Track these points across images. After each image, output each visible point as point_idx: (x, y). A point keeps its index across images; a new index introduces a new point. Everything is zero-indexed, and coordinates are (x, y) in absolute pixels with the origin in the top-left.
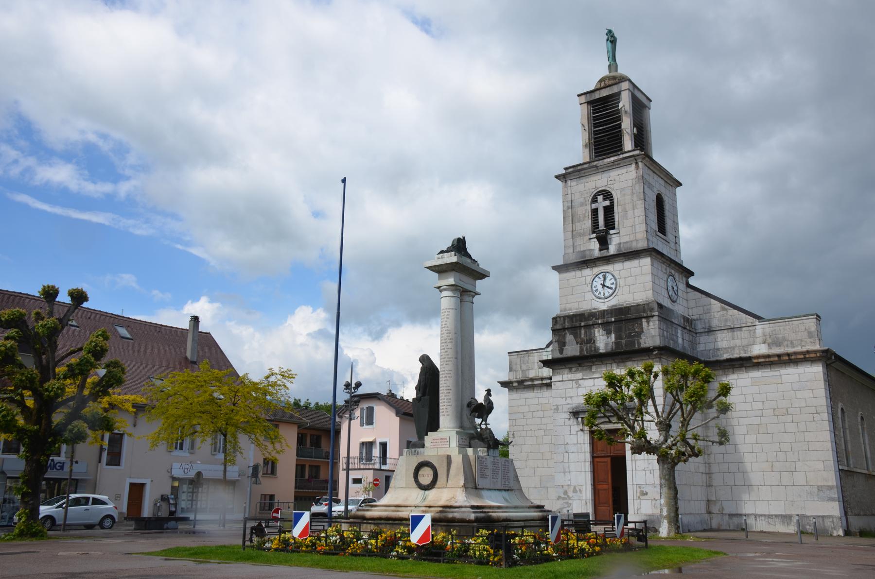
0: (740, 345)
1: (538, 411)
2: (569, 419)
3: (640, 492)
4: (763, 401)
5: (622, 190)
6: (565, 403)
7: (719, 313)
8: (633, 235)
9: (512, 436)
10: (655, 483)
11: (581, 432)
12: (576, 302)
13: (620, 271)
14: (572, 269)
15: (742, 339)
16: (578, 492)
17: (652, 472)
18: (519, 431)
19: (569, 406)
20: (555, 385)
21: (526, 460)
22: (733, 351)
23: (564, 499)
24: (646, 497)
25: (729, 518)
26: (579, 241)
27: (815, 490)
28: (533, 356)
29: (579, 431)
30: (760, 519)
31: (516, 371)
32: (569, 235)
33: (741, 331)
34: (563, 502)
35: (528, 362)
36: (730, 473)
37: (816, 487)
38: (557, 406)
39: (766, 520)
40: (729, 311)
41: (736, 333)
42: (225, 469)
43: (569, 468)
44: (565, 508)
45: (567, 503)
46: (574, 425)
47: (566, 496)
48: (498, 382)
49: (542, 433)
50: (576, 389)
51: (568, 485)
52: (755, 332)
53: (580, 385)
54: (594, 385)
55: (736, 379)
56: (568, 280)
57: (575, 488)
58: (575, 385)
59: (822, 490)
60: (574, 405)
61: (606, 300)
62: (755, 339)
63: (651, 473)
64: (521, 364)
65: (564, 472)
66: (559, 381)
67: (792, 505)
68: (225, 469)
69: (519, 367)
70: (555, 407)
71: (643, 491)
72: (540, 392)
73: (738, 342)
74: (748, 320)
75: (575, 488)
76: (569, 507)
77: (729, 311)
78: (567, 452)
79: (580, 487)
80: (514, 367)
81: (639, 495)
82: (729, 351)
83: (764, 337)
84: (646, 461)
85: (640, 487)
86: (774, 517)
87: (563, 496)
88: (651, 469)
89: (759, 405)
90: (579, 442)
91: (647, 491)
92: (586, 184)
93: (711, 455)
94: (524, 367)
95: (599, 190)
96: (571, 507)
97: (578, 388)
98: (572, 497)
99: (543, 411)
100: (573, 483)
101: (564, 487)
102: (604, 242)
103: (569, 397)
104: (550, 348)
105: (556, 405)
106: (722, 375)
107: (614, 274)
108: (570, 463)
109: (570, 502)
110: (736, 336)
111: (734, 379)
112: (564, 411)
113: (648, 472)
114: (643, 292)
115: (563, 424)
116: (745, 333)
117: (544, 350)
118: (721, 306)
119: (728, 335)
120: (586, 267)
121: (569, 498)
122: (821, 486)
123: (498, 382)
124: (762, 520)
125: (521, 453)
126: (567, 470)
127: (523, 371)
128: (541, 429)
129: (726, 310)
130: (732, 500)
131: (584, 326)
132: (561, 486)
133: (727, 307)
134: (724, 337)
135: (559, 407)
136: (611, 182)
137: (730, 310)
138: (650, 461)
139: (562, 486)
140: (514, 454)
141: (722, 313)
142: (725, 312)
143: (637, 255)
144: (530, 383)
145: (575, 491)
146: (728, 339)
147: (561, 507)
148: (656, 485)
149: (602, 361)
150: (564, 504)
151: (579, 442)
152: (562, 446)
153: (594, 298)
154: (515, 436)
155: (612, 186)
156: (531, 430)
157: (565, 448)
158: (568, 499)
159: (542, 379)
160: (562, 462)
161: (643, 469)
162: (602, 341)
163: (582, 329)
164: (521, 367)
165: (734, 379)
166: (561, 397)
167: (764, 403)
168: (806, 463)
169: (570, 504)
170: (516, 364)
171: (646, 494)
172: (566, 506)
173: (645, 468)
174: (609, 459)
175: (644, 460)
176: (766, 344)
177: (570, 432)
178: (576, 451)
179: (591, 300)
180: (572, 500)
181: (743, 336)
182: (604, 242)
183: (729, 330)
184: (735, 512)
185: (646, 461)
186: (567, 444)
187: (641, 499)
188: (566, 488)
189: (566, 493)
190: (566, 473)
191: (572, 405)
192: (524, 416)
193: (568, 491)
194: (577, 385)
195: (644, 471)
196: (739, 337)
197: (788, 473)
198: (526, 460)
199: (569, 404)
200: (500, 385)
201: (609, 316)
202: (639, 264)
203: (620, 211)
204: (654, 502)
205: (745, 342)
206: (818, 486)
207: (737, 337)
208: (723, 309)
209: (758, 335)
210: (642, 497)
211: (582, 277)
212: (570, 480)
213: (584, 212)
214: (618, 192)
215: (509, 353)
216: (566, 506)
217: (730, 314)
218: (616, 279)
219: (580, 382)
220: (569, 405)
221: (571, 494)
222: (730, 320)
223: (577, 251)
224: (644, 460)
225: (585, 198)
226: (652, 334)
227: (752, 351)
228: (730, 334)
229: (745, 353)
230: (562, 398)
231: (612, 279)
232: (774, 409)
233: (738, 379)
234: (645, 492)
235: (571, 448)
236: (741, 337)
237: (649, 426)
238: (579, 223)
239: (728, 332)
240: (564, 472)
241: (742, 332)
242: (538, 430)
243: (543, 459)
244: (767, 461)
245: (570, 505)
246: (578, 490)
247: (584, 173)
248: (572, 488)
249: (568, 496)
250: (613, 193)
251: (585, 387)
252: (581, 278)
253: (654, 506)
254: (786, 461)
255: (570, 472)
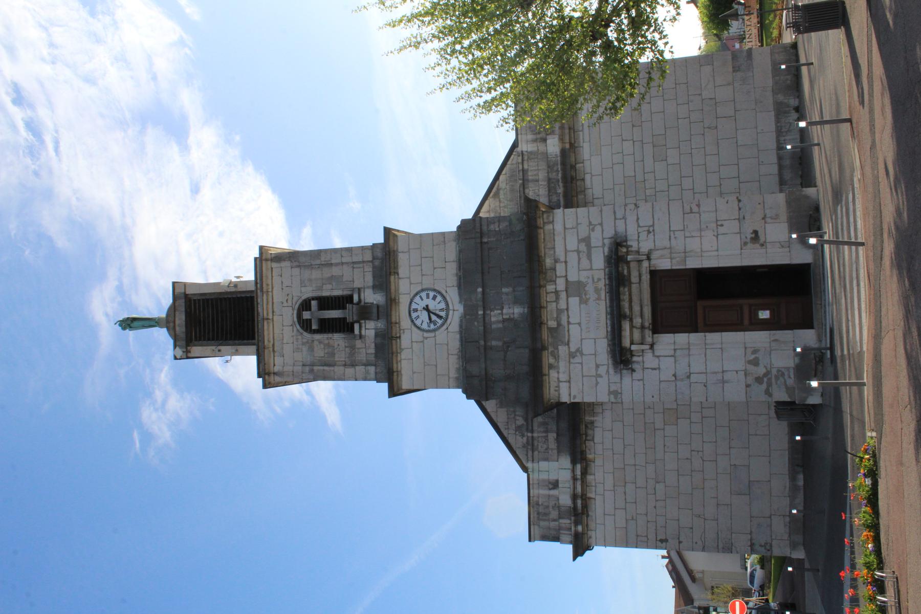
0: (546, 171)
1: (625, 493)
2: (633, 370)
3: (754, 243)
4: (623, 140)
5: (302, 284)
6: (606, 377)
7: (502, 199)
8: (365, 267)
9: (664, 544)
10: (738, 217)
11: (655, 347)
12: (448, 358)
13: (411, 284)
14: (397, 363)
15: (538, 170)
16: (757, 355)
17: (719, 223)
18: (656, 530)
19: (611, 371)
20: (575, 397)
21: (705, 519)
23: (769, 384)
25: (786, 185)
26: (362, 356)
27: (739, 74)
28: (538, 497)
29: (653, 352)
30: (783, 142)
31: (559, 529)
32: (350, 371)
33: (527, 170)
34: (774, 386)
35: (547, 507)
36: (721, 184)
37: (734, 74)
38: (610, 393)
39: (784, 134)
41: (530, 178)
44: (785, 382)
45: (777, 378)
46: (643, 362)
47: (765, 379)
48: (574, 559)
49: (660, 487)
51: (746, 375)
52: (531, 153)
53: (578, 350)
54: (579, 324)
55: (592, 176)
56: (414, 373)
57: (750, 362)
58: (578, 359)
59: (739, 67)
60: (610, 362)
61: (451, 307)
62: (540, 152)
63: (722, 225)
64: (548, 520)
65: (723, 382)
66: (570, 387)
67: (761, 102)
69: (553, 523)
71: (752, 239)
72: (596, 486)
73: (542, 175)
74: (514, 162)
75: (750, 362)
76: (783, 375)
78: (689, 377)
79: (749, 351)
80: (553, 533)
81: (757, 246)
83: (538, 140)
85: (746, 244)
86: (779, 124)
87: (764, 386)
88: (715, 225)
89: (628, 146)
90: (672, 353)
91: (751, 231)
92: (285, 341)
93: (709, 593)
94: (554, 514)
95: (296, 319)
96: (783, 370)
97: (582, 354)
98: (765, 367)
99: (626, 483)
100: (740, 365)
101: (749, 383)
102: (365, 312)
103: (597, 370)
104: (529, 465)
105: (609, 395)
107: (415, 292)
108: (708, 371)
109: (774, 372)
110: (533, 178)
111: (591, 178)
112: (619, 381)
113: (721, 230)
114: (446, 245)
115: (641, 382)
116: (530, 166)
117: (531, 476)
119: (531, 187)
120: (397, 325)
122: (733, 67)
123: (574, 559)
124: (784, 140)
125: (692, 528)
126: (720, 376)
127: (560, 517)
128: (655, 489)
129: (498, 189)
131: (485, 341)
133: (494, 189)
134: (534, 193)
135: (611, 390)
136: (290, 302)
138: (703, 226)
139: (748, 386)
140: (694, 541)
142: (501, 192)
143: (392, 254)
144: (579, 502)
145: (755, 362)
147: (785, 390)
148: (741, 217)
149: (541, 307)
150: (779, 382)
151: (672, 353)
152: (678, 384)
153: (445, 327)
154: (664, 538)
155: (295, 299)
156: (655, 507)
157: (682, 380)
158: (770, 376)
159: (574, 479)
160: (705, 386)
163: (489, 344)
164: (554, 520)
165: (591, 178)
166: (596, 386)
167: (624, 138)
168: (703, 87)
169: (778, 371)
170: (549, 528)
171: (756, 232)
173: (714, 235)
174: (700, 304)
175: (701, 237)
176: (548, 137)
177: (655, 369)
179: (448, 332)
181: (534, 168)
182: (365, 312)
183: (526, 186)
184: (777, 179)
186: (675, 375)
187: (765, 242)
188: (750, 380)
189: (759, 380)
190: (725, 378)
191: (611, 366)
192: (633, 519)
193: (757, 376)
194: (578, 354)
196: (535, 173)
197: (718, 108)
198: (705, 519)
199: (608, 371)
200: (579, 558)
202: (405, 252)
203: (329, 286)
204: (768, 220)
205: (543, 165)
206: (734, 71)
207: (535, 175)
208: (497, 195)
209: (535, 149)
210: (762, 240)
211: (412, 348)
213: (322, 346)
214: (303, 289)
215: (530, 540)
216: (781, 379)
218: (423, 290)
221: (761, 370)
222: (512, 186)
223: (374, 359)
224: (701, 237)
225: (303, 344)
226: (507, 226)
227: (556, 155)
228: (531, 185)
229: (557, 165)
230: (597, 383)
231: (421, 297)
232: (633, 126)
233: (591, 173)
235: (682, 370)
236: (535, 170)
237: (646, 229)
238: (337, 356)
239: (528, 188)
240: (723, 382)
241: (530, 169)
242: (655, 494)
243: (703, 489)
244: (703, 134)
245: (781, 373)
246: (753, 357)
247: (269, 341)
248: (751, 368)
249: (765, 375)
250: (303, 298)
252: (414, 349)
253: (775, 219)
254: (702, 110)
255: (723, 372)
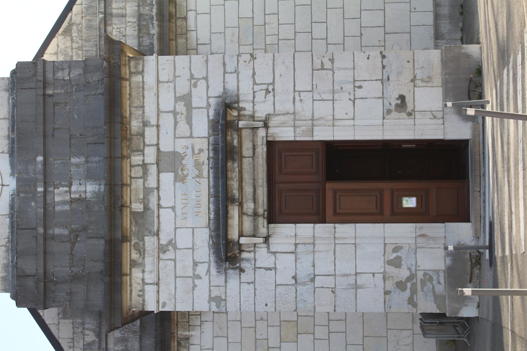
2: (242, 270)
3: (399, 112)
6: (206, 279)
7: (74, 38)
10: (380, 78)
16: (399, 254)
17: (357, 84)
19: (214, 271)
20: (164, 304)
22: (146, 17)
23: (414, 291)
24: (409, 100)
29: (268, 248)
34: (420, 294)
36: (361, 35)
38: (211, 299)
40: (73, 21)
42: (355, 234)
43: (346, 275)
44: (433, 288)
47: (409, 285)
50: (177, 251)
51: (384, 279)
53: (170, 243)
54: (173, 208)
55: (197, 14)
57: (390, 263)
58: (169, 255)
63: (360, 87)
65: (356, 287)
68: (355, 234)
70: (213, 304)
71: (397, 105)
75: (390, 263)
77: (73, 21)
78: (313, 280)
79: (389, 248)
81: (404, 115)
82: (145, 23)
84: (336, 96)
85: (389, 112)
87: (408, 293)
90: (292, 248)
96: (431, 273)
98: (409, 269)
100: (378, 266)
101: (388, 288)
103: (194, 270)
105: (209, 302)
106: (187, 39)
109: (420, 275)
110: (120, 11)
111: (196, 17)
113: (359, 93)
115: (252, 285)
118: (62, 34)
119: (116, 24)
121: (412, 277)
126: (352, 280)
129: (70, 25)
130: (410, 33)
132: (387, 296)
135: (213, 295)
137: (71, 19)
139: (387, 293)
141: (75, 34)
142: (74, 28)
145: (396, 263)
146: (124, 26)
147: (432, 298)
148: (385, 78)
149: (123, 185)
150: (425, 289)
151: (292, 248)
157: (304, 284)
158: (414, 281)
161: (351, 103)
162: (82, 188)
163: (50, 232)
165: (196, 17)
169: (425, 274)
171: (402, 98)
172: (429, 285)
173: (350, 99)
174: (330, 186)
175: (333, 100)
177: (270, 269)
178: (310, 258)
180: (416, 270)
185: (336, 96)
186: (295, 278)
187: (413, 110)
188: (390, 285)
189: (401, 285)
190: (359, 282)
191: (213, 264)
193: (397, 280)
194: (170, 248)
195: (356, 101)
199: (209, 271)
201: (31, 168)
204: (419, 83)
208: (68, 32)
210: (410, 107)
212: (373, 274)
216: (429, 285)
217: (80, 19)
219: (163, 241)
220: (211, 270)
221: (403, 273)
222: (90, 21)
224: (333, 100)
226: (80, 74)
228: (115, 20)
230: (195, 286)
233: (196, 10)
234: (399, 102)
237: (265, 87)
240: (356, 287)
245: (428, 277)
246: (394, 255)
248: (391, 270)
249: (409, 279)
251: (176, 229)
253: (427, 82)
255: (356, 274)
